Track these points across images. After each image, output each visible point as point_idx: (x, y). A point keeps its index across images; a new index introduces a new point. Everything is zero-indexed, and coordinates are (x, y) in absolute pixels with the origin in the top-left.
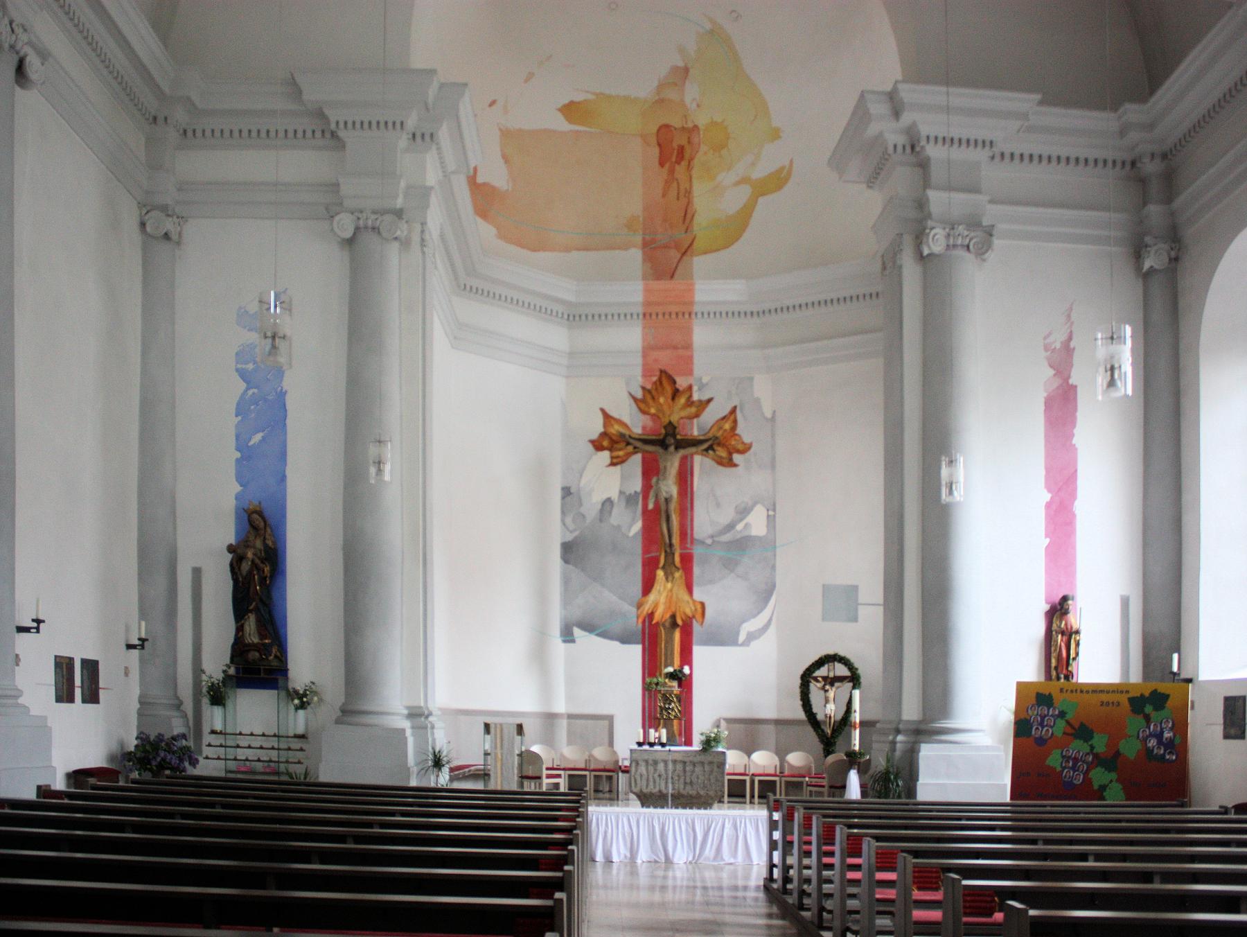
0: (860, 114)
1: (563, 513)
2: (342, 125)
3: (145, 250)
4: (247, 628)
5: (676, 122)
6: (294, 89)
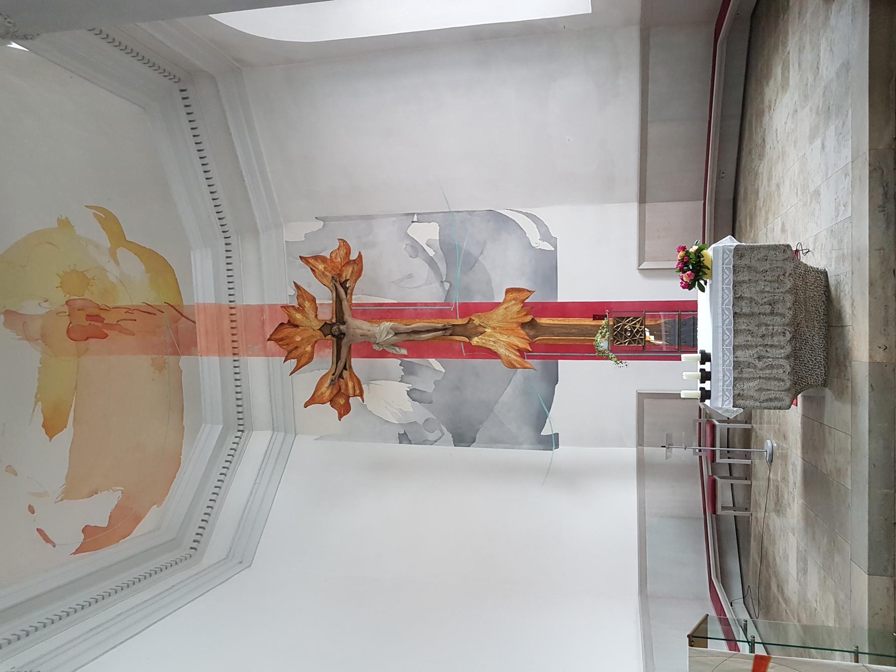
1: (424, 442)
5: (64, 322)
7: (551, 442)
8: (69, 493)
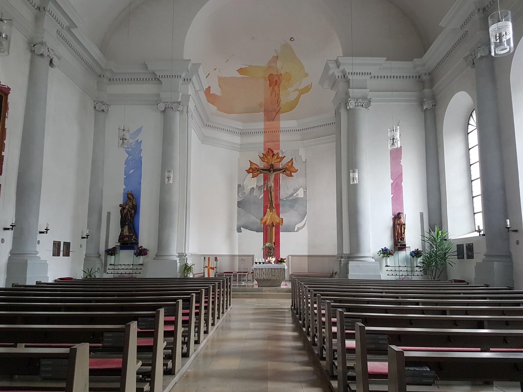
0: (327, 68)
2: (161, 76)
3: (95, 115)
4: (125, 230)
5: (275, 73)
6: (145, 67)
7: (239, 230)
8: (220, 79)
